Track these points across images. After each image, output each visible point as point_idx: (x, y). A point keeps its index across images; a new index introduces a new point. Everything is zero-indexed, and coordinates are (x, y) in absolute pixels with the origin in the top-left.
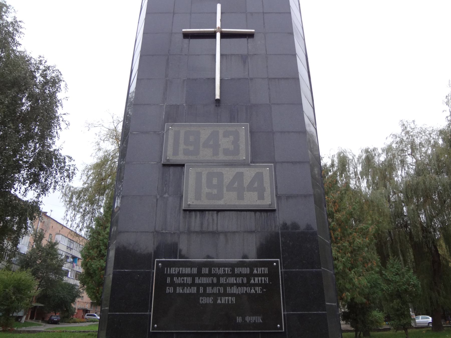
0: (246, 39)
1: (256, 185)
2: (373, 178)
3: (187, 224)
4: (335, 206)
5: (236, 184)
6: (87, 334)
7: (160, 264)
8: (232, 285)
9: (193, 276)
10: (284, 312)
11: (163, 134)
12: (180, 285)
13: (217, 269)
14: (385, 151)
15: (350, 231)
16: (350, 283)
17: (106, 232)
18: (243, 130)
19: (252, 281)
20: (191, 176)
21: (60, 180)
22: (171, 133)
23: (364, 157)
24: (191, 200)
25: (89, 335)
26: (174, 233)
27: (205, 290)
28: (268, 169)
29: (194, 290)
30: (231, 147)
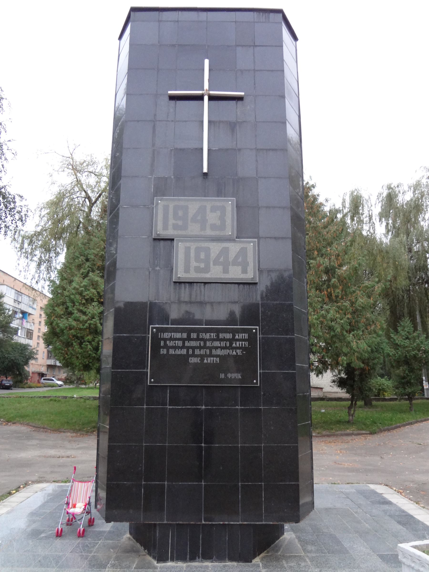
0: (234, 102)
1: (240, 260)
2: (394, 221)
3: (177, 295)
4: (337, 259)
5: (222, 258)
6: (50, 399)
7: (154, 330)
8: (216, 348)
9: (183, 340)
10: (260, 370)
11: (153, 208)
12: (172, 347)
13: (204, 334)
14: (412, 188)
15: (354, 289)
16: (347, 346)
17: (73, 287)
18: (229, 204)
19: (234, 345)
20: (180, 248)
21: (11, 224)
22: (160, 207)
23: (385, 195)
24: (180, 274)
25: (51, 400)
26: (166, 303)
27: (193, 352)
28: (252, 244)
29: (184, 352)
30: (218, 223)
